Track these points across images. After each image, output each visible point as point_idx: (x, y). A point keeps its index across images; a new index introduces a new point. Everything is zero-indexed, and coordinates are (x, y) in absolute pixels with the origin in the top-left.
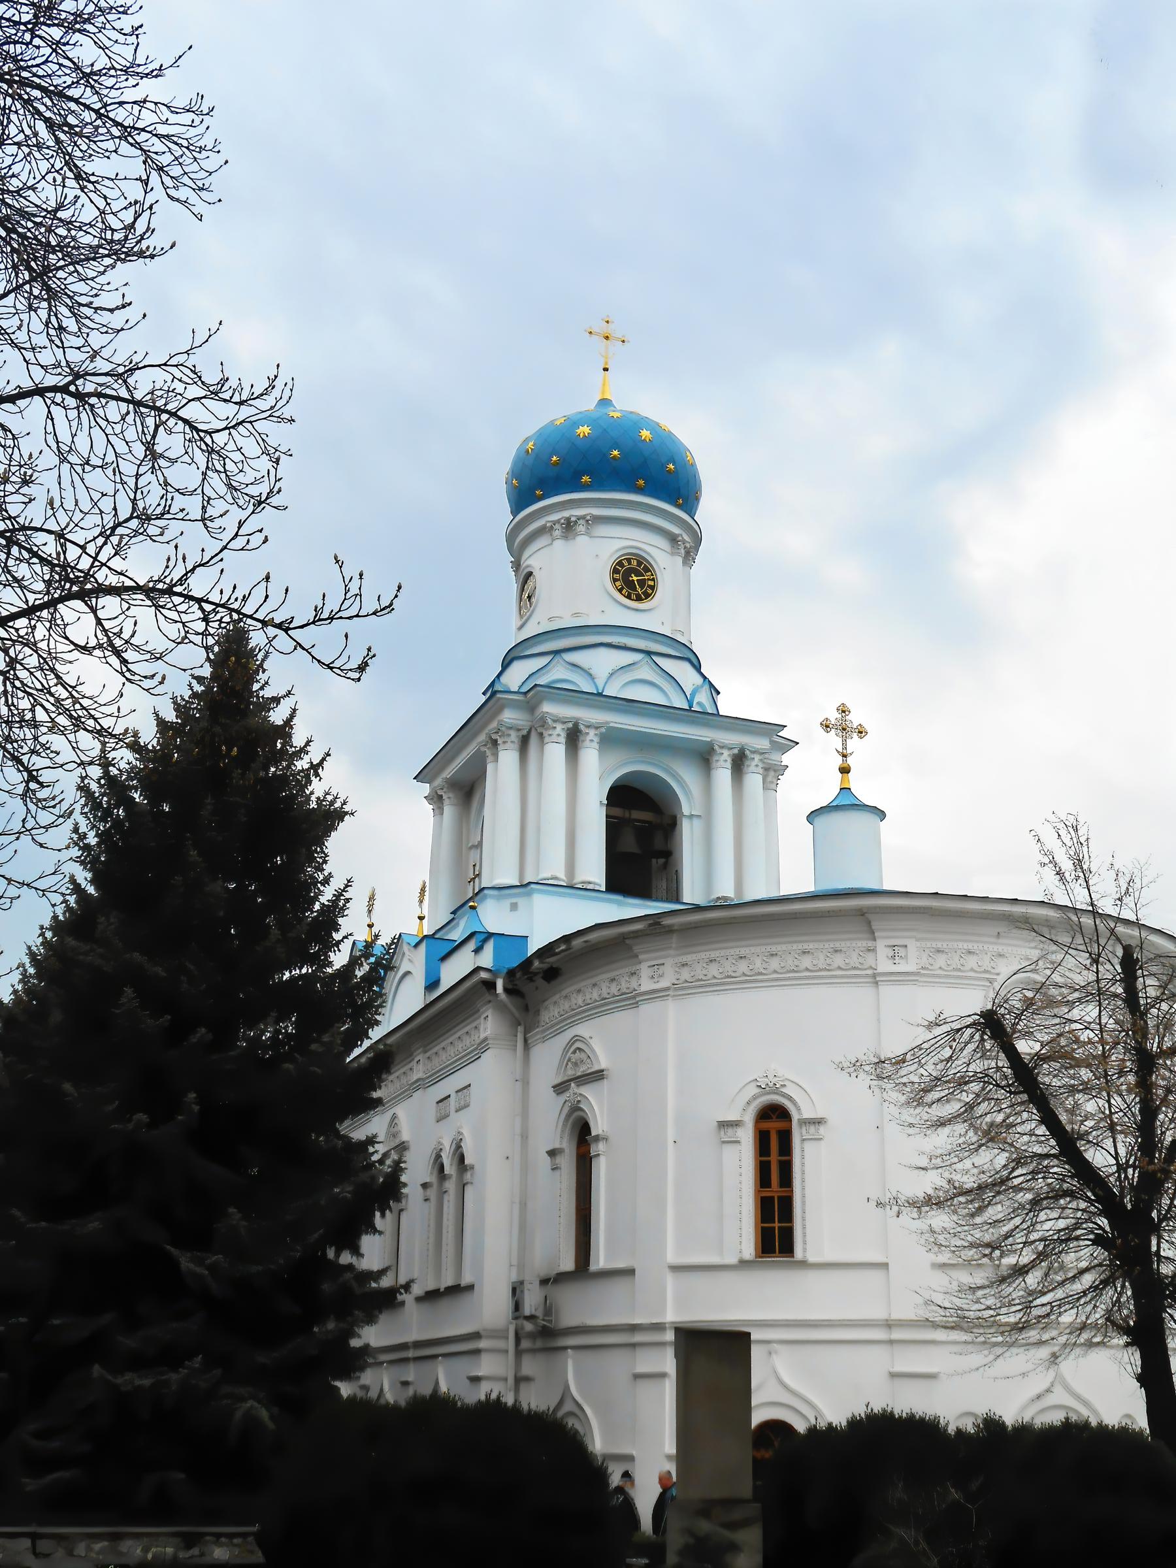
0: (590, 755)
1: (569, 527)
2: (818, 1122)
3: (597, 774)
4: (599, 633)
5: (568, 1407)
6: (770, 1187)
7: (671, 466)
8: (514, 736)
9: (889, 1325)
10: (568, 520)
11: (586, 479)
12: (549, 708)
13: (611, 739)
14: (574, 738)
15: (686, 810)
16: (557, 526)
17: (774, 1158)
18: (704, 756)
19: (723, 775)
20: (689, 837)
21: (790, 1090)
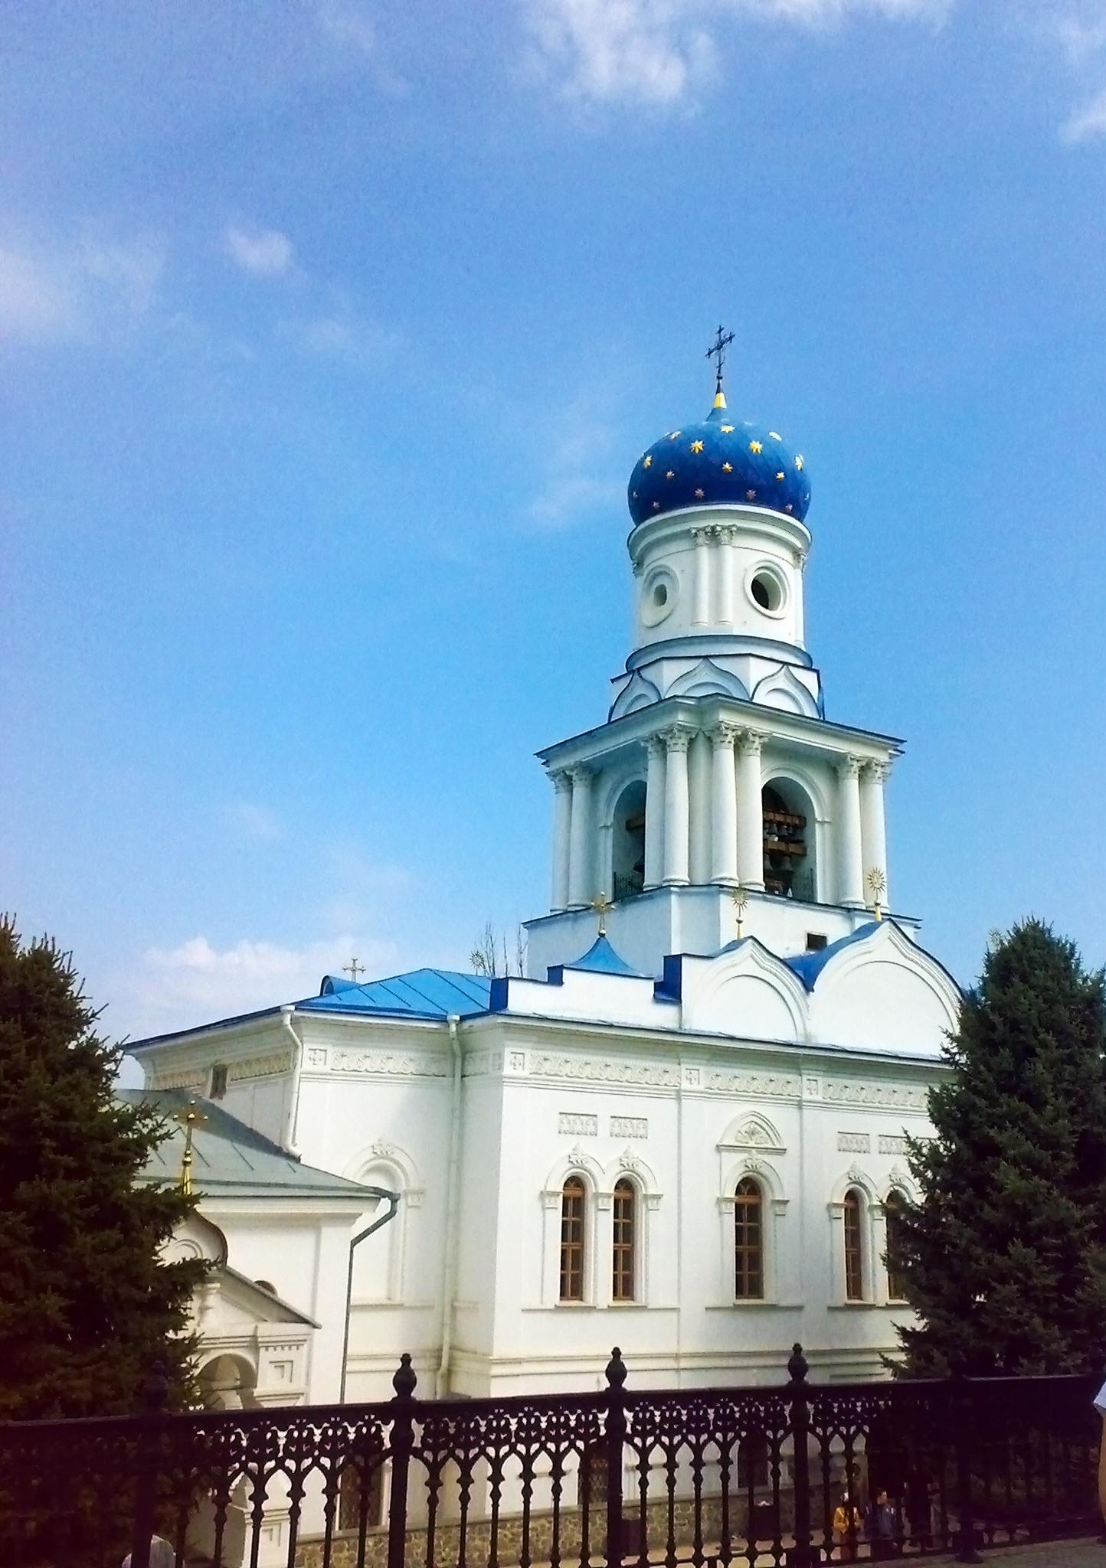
1: (713, 536)
2: (658, 1197)
3: (759, 773)
4: (652, 653)
5: (651, 1204)
7: (781, 475)
8: (684, 740)
9: (677, 1357)
10: (713, 528)
11: (751, 493)
12: (725, 717)
13: (773, 749)
14: (741, 742)
16: (702, 533)
17: (570, 1272)
18: (834, 767)
19: (852, 784)
20: (820, 840)
21: (641, 1169)
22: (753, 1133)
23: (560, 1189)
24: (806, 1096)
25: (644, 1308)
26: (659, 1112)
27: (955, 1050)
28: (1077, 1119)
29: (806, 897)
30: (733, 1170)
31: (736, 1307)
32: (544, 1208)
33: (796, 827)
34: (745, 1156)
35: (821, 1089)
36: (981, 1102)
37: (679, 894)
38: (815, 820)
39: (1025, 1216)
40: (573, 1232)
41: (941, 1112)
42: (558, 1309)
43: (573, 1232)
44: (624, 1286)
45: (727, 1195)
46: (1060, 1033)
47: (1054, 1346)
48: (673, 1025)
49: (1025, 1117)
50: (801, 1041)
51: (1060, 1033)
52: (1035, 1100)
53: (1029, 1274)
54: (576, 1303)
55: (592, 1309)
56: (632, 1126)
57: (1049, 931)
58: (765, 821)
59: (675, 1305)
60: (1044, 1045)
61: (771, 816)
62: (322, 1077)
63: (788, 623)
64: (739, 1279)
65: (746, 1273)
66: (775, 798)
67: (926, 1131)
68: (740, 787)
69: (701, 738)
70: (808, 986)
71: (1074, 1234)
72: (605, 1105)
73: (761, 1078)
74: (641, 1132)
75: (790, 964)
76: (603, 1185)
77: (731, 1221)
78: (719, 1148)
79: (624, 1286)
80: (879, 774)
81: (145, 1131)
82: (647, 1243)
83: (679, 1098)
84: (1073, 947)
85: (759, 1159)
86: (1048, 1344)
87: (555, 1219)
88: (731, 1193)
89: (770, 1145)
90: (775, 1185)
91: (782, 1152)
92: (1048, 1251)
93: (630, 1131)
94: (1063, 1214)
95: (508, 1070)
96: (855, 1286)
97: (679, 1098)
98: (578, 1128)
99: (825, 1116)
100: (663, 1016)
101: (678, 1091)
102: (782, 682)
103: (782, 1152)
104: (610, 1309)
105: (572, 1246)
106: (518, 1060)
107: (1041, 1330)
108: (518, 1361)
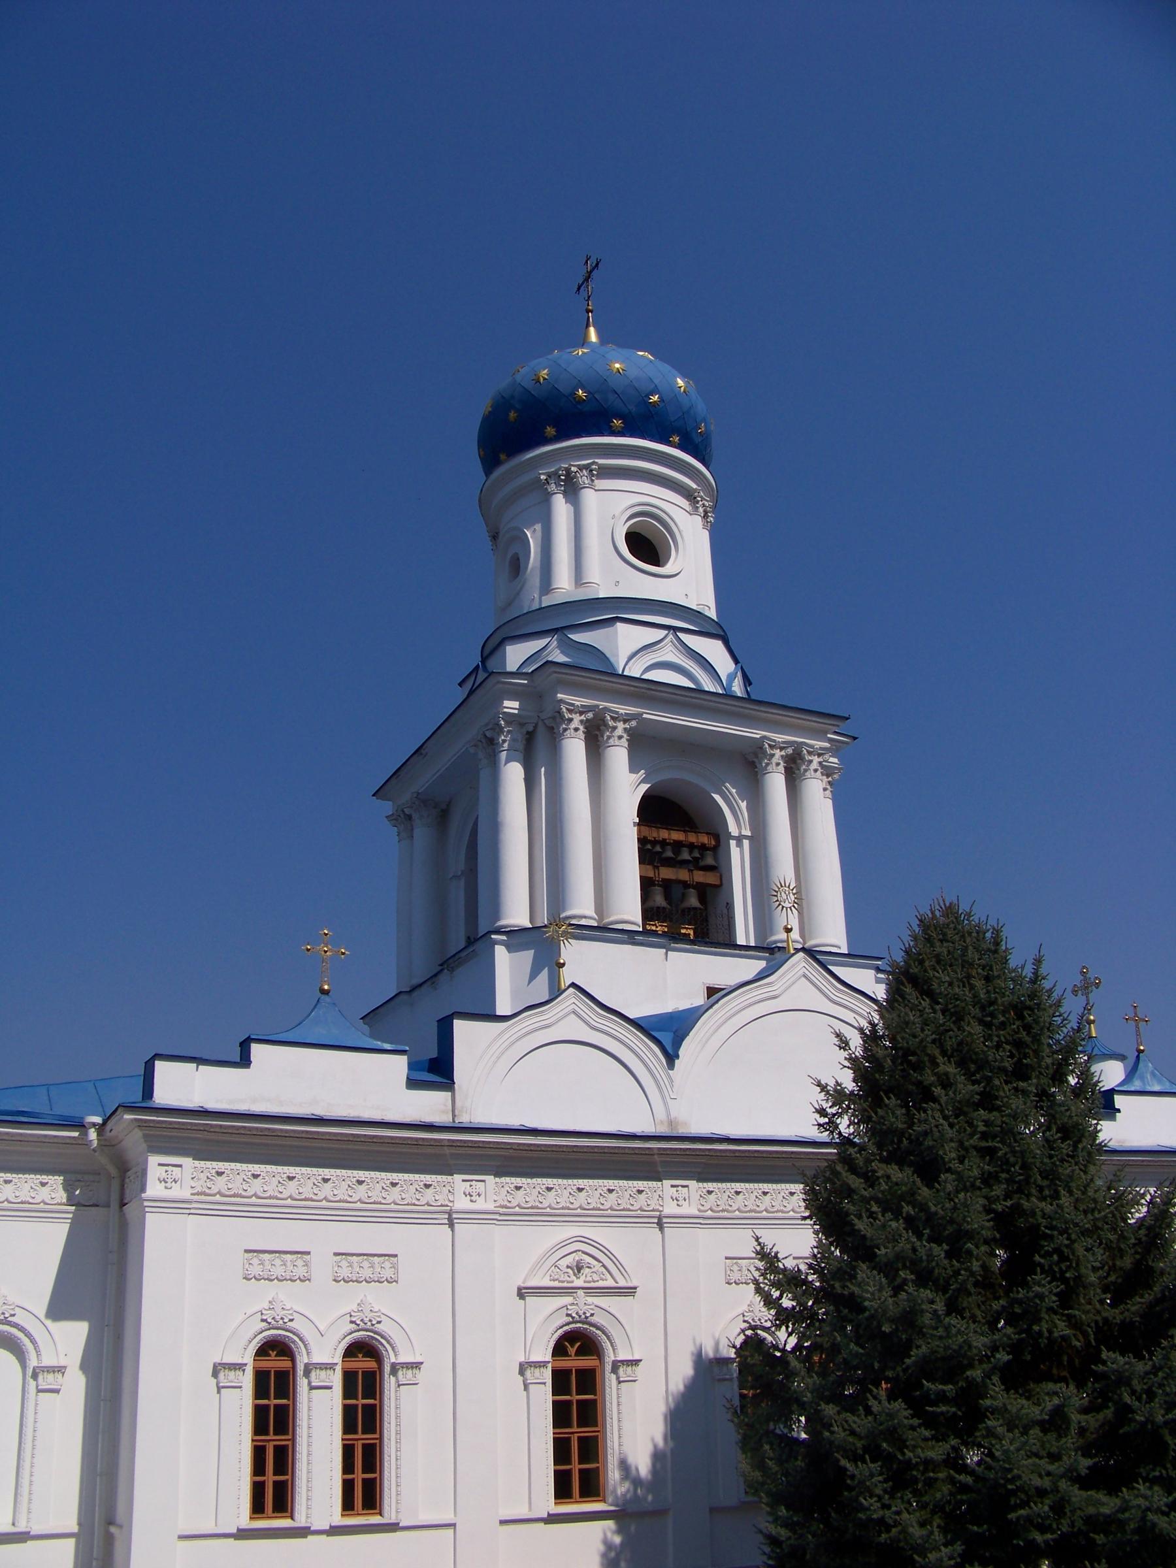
0: (618, 756)
7: (655, 398)
15: (733, 829)
17: (576, 1467)
19: (776, 782)
22: (579, 1268)
24: (670, 1209)
25: (393, 1527)
26: (422, 1246)
27: (834, 1110)
28: (998, 1190)
29: (724, 942)
30: (542, 1326)
31: (552, 1519)
32: (219, 1389)
33: (703, 848)
34: (568, 1300)
35: (695, 1196)
36: (855, 1182)
37: (510, 948)
38: (730, 836)
39: (895, 1349)
40: (274, 1420)
41: (828, 1213)
42: (242, 1534)
43: (274, 1420)
44: (363, 1488)
45: (535, 1358)
46: (966, 1059)
47: (932, 1556)
48: (444, 1119)
49: (910, 1196)
50: (663, 1130)
51: (966, 1059)
52: (929, 1169)
53: (902, 1444)
54: (375, 1519)
55: (303, 1532)
56: (381, 1266)
57: (969, 915)
58: (642, 841)
59: (448, 1517)
60: (946, 1083)
61: (646, 832)
63: (690, 576)
64: (348, 1488)
66: (655, 810)
67: (798, 1244)
68: (604, 799)
69: (541, 730)
70: (671, 1058)
71: (976, 1373)
72: (323, 1239)
73: (593, 1191)
74: (301, 1271)
75: (644, 1027)
76: (322, 1348)
77: (544, 1397)
78: (522, 1293)
79: (363, 1488)
80: (815, 765)
81: (1014, 1410)
82: (398, 1433)
83: (451, 1225)
84: (997, 932)
85: (586, 1304)
86: (923, 1553)
87: (241, 1403)
88: (543, 1353)
89: (610, 1283)
91: (630, 1291)
92: (934, 1403)
94: (955, 1342)
95: (154, 1189)
96: (273, 1491)
99: (704, 1236)
100: (428, 1105)
101: (450, 1213)
102: (669, 653)
103: (630, 1291)
104: (334, 1531)
105: (575, 1432)
106: (167, 1177)
107: (916, 1532)
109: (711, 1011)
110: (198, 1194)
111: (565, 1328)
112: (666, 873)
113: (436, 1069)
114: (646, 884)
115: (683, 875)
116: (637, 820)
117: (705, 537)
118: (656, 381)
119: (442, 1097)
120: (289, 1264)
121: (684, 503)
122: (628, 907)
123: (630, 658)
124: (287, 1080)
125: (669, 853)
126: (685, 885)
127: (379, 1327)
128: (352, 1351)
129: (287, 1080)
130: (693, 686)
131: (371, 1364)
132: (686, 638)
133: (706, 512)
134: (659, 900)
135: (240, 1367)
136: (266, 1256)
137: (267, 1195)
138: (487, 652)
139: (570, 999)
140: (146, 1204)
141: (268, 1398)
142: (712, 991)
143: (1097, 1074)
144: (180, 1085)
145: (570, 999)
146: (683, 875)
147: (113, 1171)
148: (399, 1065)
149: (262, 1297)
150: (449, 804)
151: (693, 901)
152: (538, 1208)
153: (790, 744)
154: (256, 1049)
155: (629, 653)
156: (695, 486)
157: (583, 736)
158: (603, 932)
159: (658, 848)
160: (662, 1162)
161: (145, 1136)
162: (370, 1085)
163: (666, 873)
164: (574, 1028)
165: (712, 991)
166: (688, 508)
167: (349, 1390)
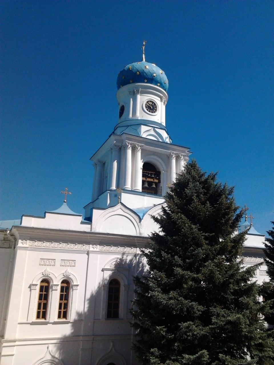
2: (77, 285)
6: (63, 300)
11: (159, 84)
17: (42, 310)
21: (71, 277)
23: (60, 283)
62: (26, 248)
65: (62, 310)
72: (59, 256)
76: (57, 282)
83: (88, 254)
87: (36, 293)
90: (74, 281)
93: (68, 264)
97: (88, 254)
98: (48, 263)
100: (86, 228)
108: (14, 341)
109: (150, 210)
110: (30, 246)
111: (43, 278)
112: (148, 179)
113: (88, 219)
114: (143, 182)
115: (152, 180)
116: (142, 168)
117: (164, 107)
118: (155, 71)
119: (89, 226)
120: (66, 262)
121: (159, 99)
122: (139, 187)
123: (144, 133)
124: (53, 221)
125: (150, 175)
126: (152, 182)
127: (69, 277)
128: (63, 282)
129: (53, 221)
130: (157, 140)
131: (46, 284)
132: (156, 129)
133: (165, 102)
134: (146, 185)
135: (58, 285)
136: (45, 260)
137: (38, 246)
138: (115, 129)
139: (119, 206)
140: (18, 248)
141: (43, 292)
142: (154, 205)
143: (239, 225)
144: (29, 222)
145: (119, 206)
146: (152, 180)
147: (13, 240)
148: (80, 219)
149: (43, 269)
150: (105, 162)
151: (154, 186)
152: (116, 251)
153: (177, 154)
154: (47, 214)
155: (143, 132)
156: (162, 95)
157: (175, 159)
158: (133, 192)
159: (147, 174)
160: (137, 242)
161: (19, 233)
162: (73, 223)
163: (148, 179)
164: (120, 212)
165: (154, 205)
166: (160, 100)
167: (62, 291)
